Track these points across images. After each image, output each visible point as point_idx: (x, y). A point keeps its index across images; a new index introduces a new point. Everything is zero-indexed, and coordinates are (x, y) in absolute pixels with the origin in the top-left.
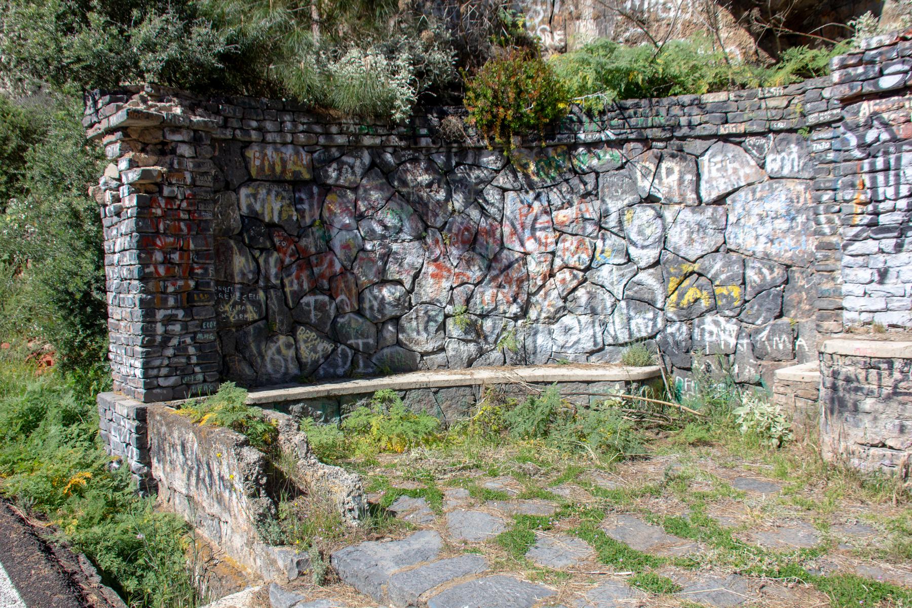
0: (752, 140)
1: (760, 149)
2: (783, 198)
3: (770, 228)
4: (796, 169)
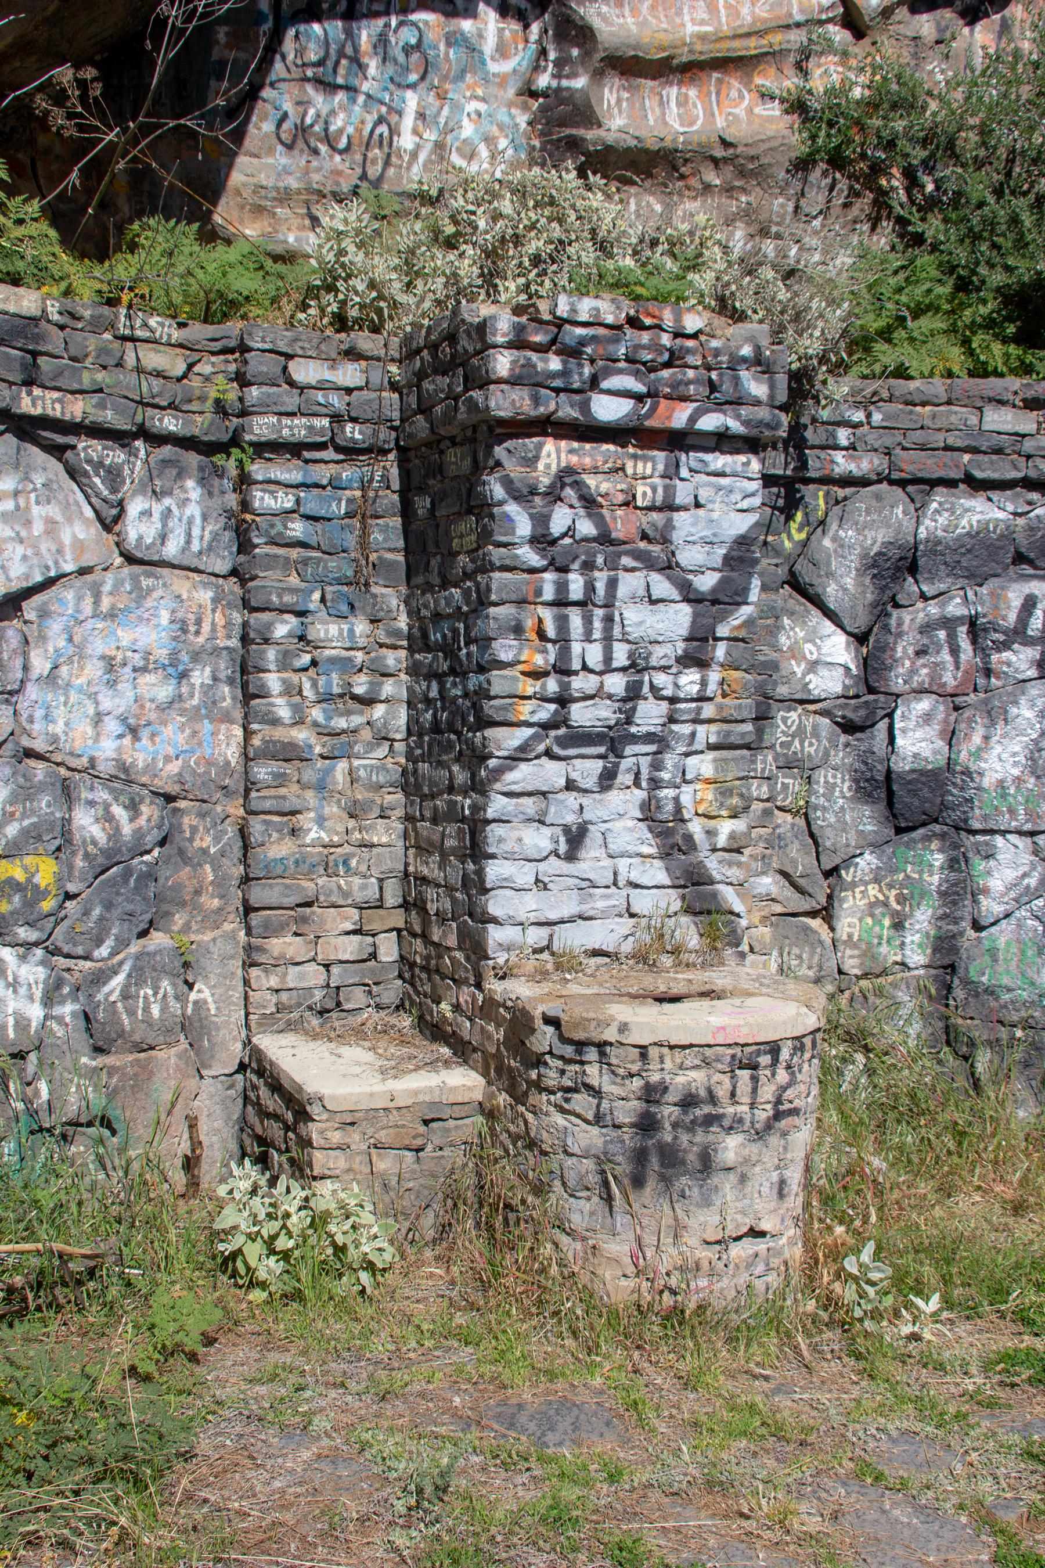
0: (89, 448)
1: (114, 476)
2: (165, 617)
3: (130, 694)
4: (195, 546)
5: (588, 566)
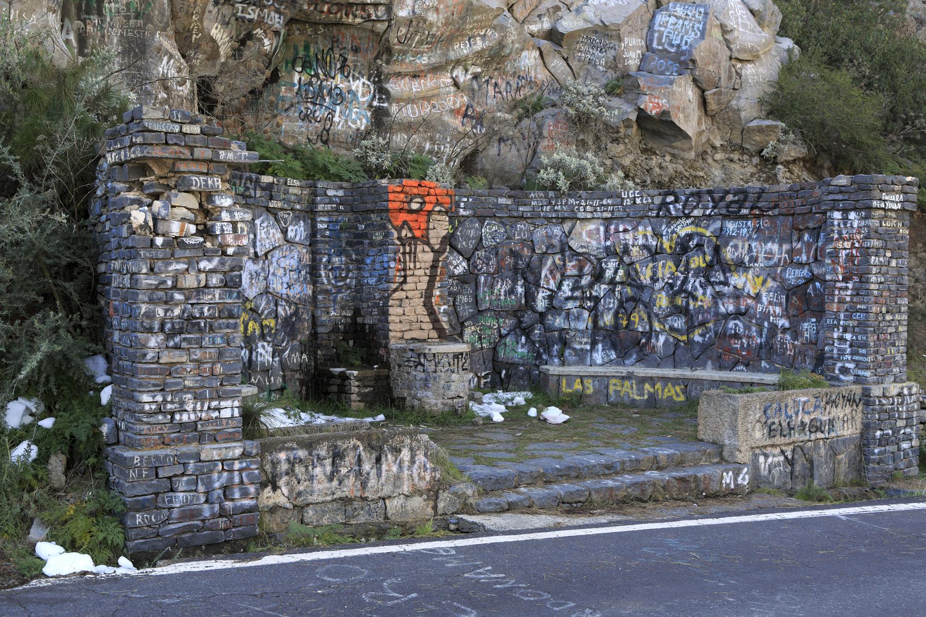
5: (410, 245)
